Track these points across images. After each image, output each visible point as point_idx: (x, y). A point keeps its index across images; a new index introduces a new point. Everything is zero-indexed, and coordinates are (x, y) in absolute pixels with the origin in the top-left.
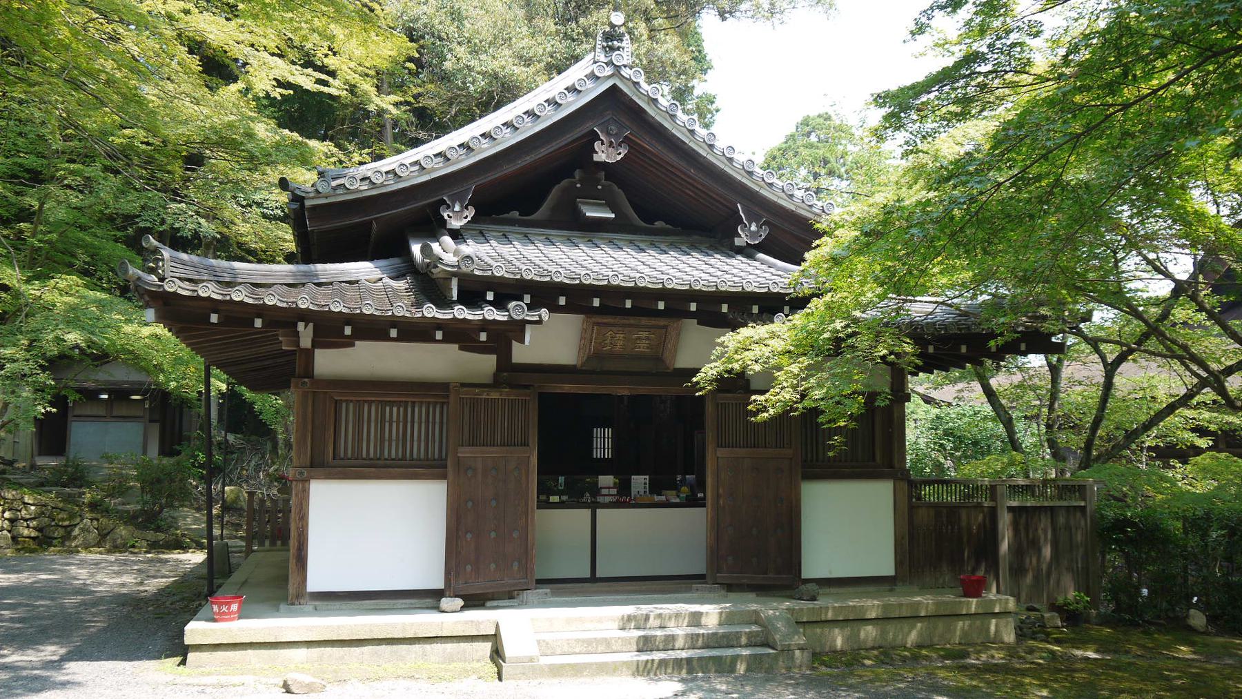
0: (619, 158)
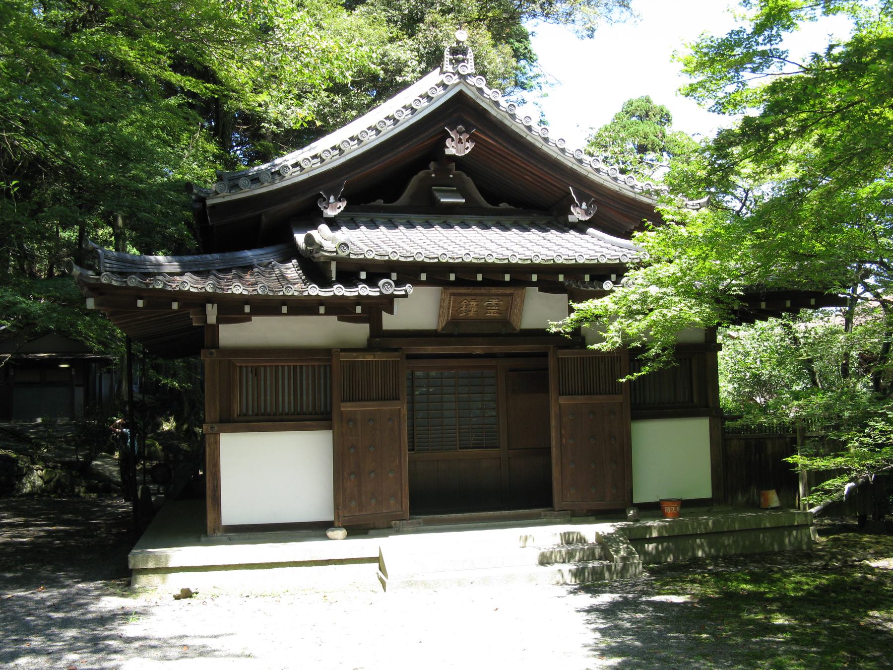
0: (467, 152)
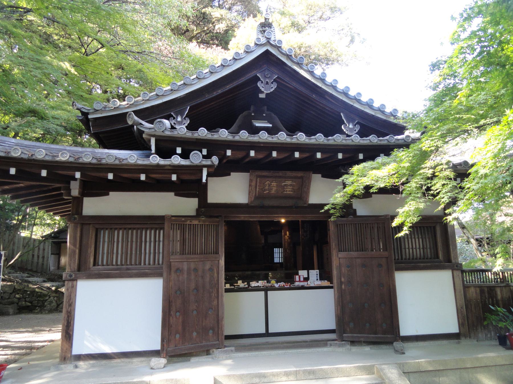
0: (272, 90)
